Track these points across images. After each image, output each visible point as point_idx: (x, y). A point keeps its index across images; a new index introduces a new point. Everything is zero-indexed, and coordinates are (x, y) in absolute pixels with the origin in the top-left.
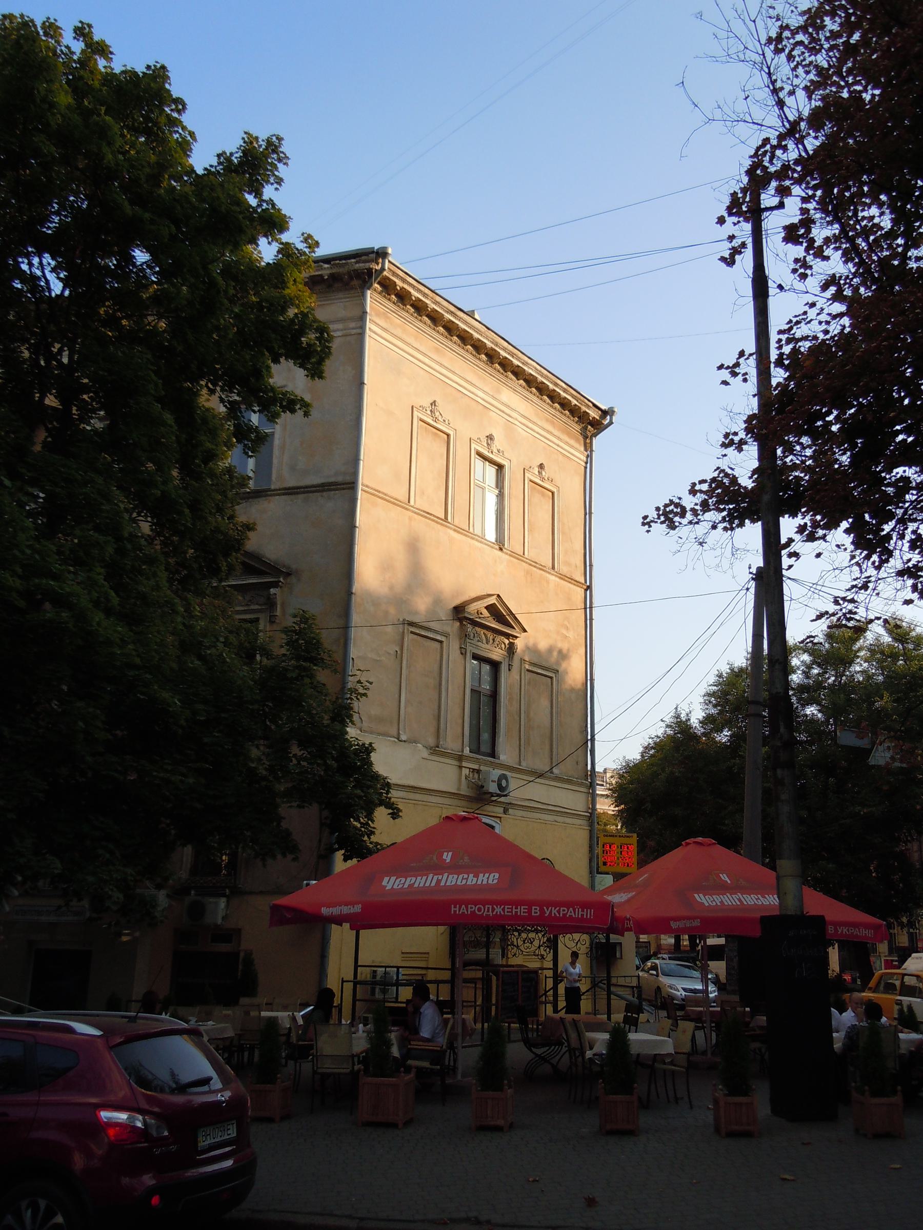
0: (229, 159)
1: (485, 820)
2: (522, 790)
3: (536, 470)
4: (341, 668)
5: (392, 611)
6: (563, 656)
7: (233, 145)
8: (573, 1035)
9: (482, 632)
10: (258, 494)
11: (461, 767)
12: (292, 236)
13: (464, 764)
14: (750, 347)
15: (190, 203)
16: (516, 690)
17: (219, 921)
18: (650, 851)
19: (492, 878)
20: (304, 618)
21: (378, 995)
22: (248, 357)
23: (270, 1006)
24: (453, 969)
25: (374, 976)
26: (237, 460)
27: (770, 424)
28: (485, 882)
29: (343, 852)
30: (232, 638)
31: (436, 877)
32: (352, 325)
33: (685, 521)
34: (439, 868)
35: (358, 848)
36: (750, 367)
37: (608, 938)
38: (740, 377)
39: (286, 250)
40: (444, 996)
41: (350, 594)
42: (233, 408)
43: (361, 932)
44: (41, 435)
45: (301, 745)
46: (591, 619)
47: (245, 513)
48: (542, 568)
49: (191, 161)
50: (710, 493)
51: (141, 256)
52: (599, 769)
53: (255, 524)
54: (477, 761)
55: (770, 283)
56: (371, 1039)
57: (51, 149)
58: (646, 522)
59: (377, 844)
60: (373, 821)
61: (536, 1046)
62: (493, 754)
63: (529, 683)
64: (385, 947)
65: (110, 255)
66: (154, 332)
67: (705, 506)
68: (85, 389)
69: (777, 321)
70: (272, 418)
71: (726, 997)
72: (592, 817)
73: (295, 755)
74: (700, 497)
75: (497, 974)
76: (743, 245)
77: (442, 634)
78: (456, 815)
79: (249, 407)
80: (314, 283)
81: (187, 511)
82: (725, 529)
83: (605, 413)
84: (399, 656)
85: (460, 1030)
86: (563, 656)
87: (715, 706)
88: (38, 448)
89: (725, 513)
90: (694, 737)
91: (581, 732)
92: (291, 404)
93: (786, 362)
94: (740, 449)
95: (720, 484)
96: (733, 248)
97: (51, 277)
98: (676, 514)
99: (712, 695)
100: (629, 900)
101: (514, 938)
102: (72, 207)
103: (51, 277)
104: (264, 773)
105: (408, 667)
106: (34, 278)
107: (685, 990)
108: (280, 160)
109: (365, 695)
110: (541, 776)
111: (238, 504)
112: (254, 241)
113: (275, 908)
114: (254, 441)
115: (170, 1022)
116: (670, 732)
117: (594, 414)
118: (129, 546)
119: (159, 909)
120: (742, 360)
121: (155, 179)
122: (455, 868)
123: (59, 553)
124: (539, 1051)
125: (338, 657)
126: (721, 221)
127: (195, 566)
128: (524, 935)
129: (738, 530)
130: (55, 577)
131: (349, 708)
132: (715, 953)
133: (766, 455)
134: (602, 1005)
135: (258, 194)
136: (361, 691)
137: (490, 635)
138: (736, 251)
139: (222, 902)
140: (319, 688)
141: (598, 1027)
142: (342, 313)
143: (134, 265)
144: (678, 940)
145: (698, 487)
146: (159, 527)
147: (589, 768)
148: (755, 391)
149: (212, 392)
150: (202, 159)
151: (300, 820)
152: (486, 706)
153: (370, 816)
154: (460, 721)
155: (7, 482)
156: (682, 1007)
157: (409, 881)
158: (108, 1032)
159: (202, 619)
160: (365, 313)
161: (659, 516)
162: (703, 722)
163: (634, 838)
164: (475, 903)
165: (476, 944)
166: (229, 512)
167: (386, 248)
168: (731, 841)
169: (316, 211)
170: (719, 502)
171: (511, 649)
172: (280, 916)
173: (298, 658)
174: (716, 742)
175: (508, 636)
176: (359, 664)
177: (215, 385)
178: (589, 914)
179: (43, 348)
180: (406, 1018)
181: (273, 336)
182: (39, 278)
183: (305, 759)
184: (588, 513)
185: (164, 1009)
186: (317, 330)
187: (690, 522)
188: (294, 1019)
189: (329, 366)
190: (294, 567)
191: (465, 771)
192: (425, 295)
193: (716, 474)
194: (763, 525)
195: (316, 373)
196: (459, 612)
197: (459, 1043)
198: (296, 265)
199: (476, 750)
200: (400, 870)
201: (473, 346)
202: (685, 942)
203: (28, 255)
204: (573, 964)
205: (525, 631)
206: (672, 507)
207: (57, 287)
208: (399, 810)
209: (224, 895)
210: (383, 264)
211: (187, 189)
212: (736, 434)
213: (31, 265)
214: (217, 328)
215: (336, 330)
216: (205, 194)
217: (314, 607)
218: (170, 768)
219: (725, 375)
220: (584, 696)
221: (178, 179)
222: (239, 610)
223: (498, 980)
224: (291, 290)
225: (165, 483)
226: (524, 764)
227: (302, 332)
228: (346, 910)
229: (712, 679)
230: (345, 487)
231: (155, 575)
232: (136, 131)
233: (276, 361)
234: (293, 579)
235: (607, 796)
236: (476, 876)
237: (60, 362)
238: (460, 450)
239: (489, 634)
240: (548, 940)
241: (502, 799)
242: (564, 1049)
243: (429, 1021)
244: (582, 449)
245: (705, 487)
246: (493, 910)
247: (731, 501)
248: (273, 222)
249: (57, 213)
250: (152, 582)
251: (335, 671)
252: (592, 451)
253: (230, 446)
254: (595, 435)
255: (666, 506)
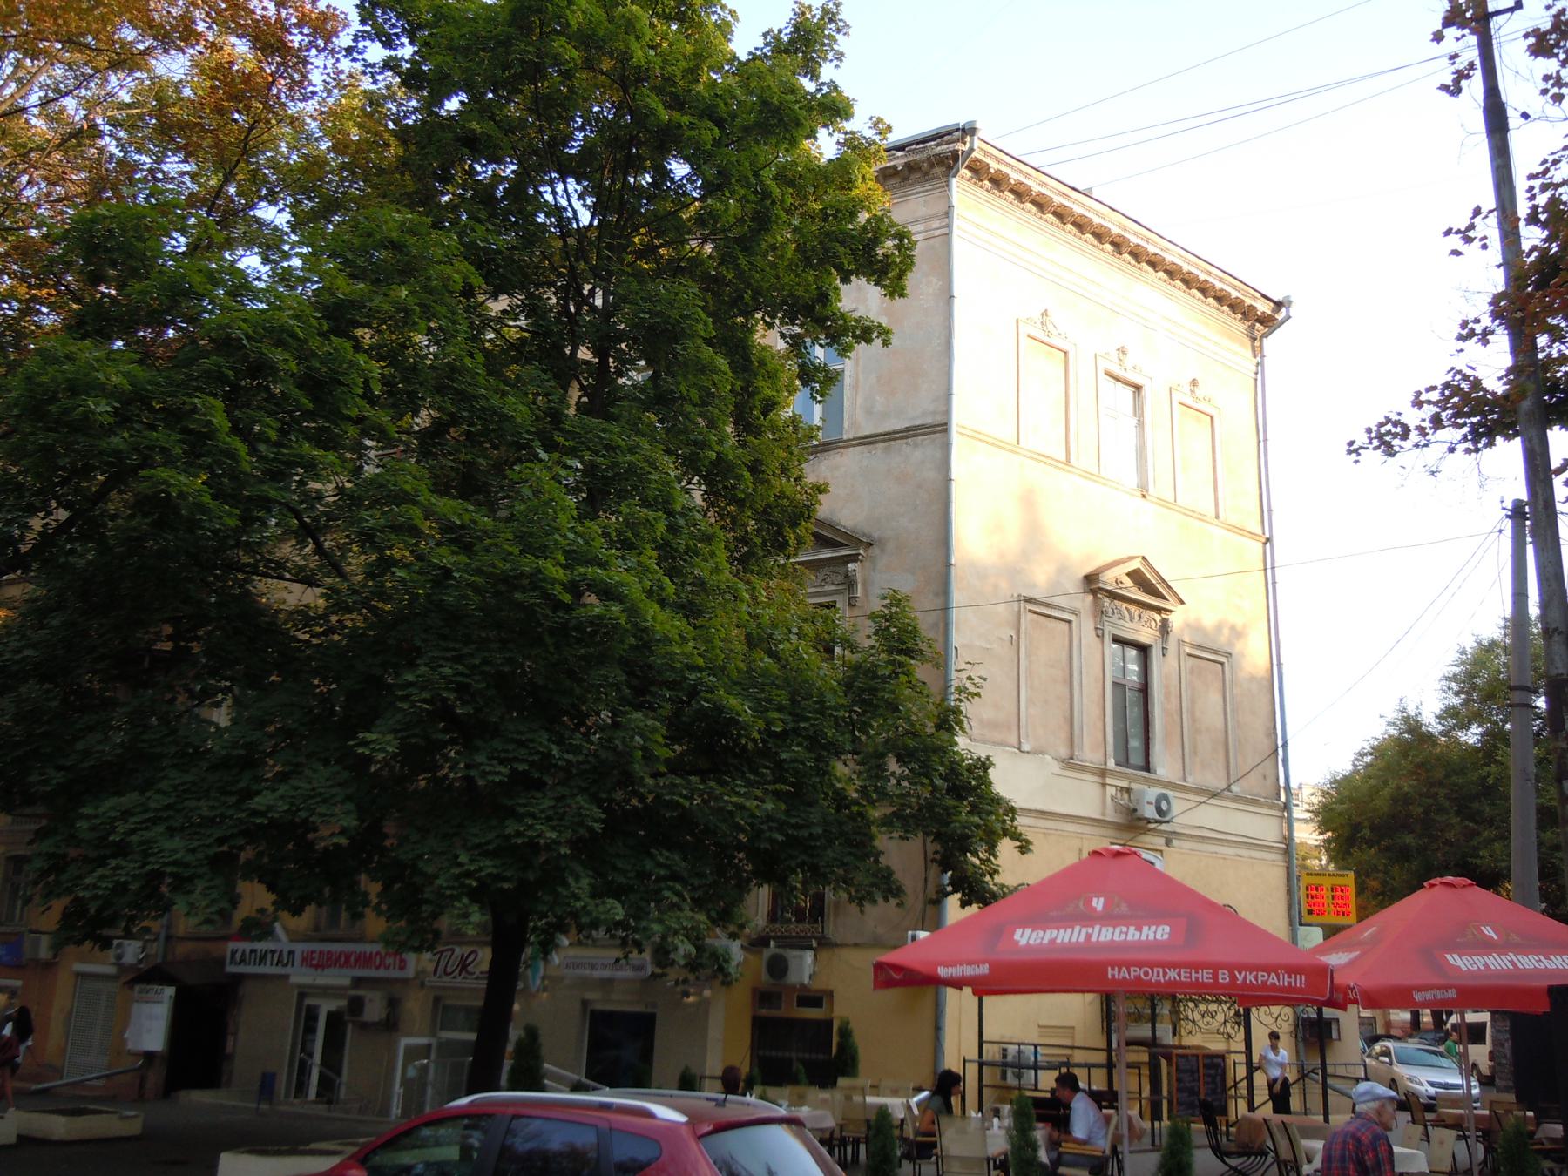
0: (777, 39)
1: (1145, 855)
2: (1186, 814)
3: (1187, 387)
4: (941, 662)
5: (1004, 584)
6: (1237, 633)
7: (780, 19)
8: (1283, 1144)
9: (1123, 606)
10: (827, 447)
11: (1104, 785)
12: (859, 123)
13: (1109, 781)
14: (1489, 201)
15: (734, 97)
16: (1175, 682)
17: (806, 981)
18: (1379, 893)
19: (1162, 932)
20: (896, 600)
21: (1011, 1080)
22: (811, 279)
23: (876, 1089)
24: (1109, 1049)
25: (1005, 1056)
26: (800, 406)
27: (1528, 301)
28: (1151, 937)
29: (959, 895)
30: (809, 629)
31: (1084, 931)
32: (936, 224)
33: (1408, 444)
34: (1089, 918)
35: (975, 891)
36: (1489, 228)
37: (1320, 1012)
38: (1477, 243)
39: (852, 143)
40: (1099, 1084)
41: (948, 565)
42: (796, 344)
43: (986, 999)
44: (575, 393)
45: (900, 759)
46: (1274, 583)
47: (816, 471)
48: (1202, 518)
49: (732, 46)
50: (1443, 403)
51: (679, 169)
52: (1294, 785)
53: (827, 484)
54: (1126, 777)
55: (1510, 113)
56: (1011, 1137)
57: (572, 54)
58: (1353, 450)
59: (1003, 886)
60: (996, 857)
61: (1229, 1154)
62: (1147, 767)
63: (1192, 672)
64: (1019, 1020)
65: (639, 171)
66: (697, 262)
67: (1437, 422)
68: (621, 337)
69: (1524, 162)
70: (844, 352)
71: (1493, 1095)
72: (1288, 847)
73: (893, 773)
74: (1429, 410)
75: (1168, 1057)
76: (1472, 66)
77: (1070, 612)
78: (1107, 850)
79: (815, 340)
80: (886, 176)
81: (747, 474)
82: (1468, 451)
83: (1278, 305)
84: (1015, 642)
85: (1125, 1131)
86: (1237, 633)
87: (1457, 694)
88: (572, 411)
89: (1466, 430)
90: (1430, 737)
91: (1268, 736)
92: (866, 332)
93: (1543, 217)
94: (1484, 341)
95: (1457, 391)
96: (1458, 72)
97: (577, 205)
98: (1395, 435)
99: (1454, 678)
100: (1351, 963)
101: (1189, 1010)
102: (597, 119)
103: (577, 205)
104: (855, 795)
105: (1028, 656)
106: (558, 210)
107: (1432, 1084)
108: (839, 31)
109: (978, 695)
110: (1215, 795)
111: (806, 461)
112: (812, 135)
113: (879, 967)
114: (820, 381)
115: (755, 1106)
116: (1393, 731)
117: (1263, 307)
118: (682, 522)
119: (734, 964)
120: (1477, 221)
121: (693, 73)
122: (1109, 918)
123: (605, 535)
124: (1234, 1162)
125: (938, 646)
126: (1438, 37)
127: (758, 541)
128: (1202, 1007)
129: (1486, 452)
130: (603, 565)
131: (957, 712)
132: (1475, 1034)
133: (1522, 345)
134: (1315, 1100)
135: (814, 75)
136: (972, 689)
137: (1134, 610)
138: (1461, 75)
139: (809, 957)
140: (918, 688)
141: (1311, 1133)
142: (923, 211)
143: (672, 179)
144: (1416, 1016)
145: (1424, 397)
146: (711, 495)
147: (1282, 783)
148: (1499, 260)
149: (770, 326)
150: (745, 42)
151: (902, 854)
152: (1136, 706)
153: (992, 849)
154: (1100, 725)
155: (543, 455)
156: (1430, 1108)
157: (1050, 935)
158: (694, 1119)
159: (769, 606)
160: (951, 207)
161: (1371, 439)
162: (1441, 717)
163: (1349, 879)
164: (1140, 965)
165: (1138, 1018)
166: (795, 473)
167: (973, 122)
168: (1490, 880)
169: (884, 86)
170: (1456, 415)
171: (1164, 628)
172: (890, 977)
173: (890, 651)
174: (1460, 744)
175: (1159, 610)
176: (965, 655)
177: (773, 317)
178: (1299, 981)
179: (571, 291)
180: (1054, 1111)
181: (842, 250)
182: (565, 209)
183: (906, 778)
184: (1262, 441)
185: (749, 1087)
186: (895, 236)
187: (1417, 446)
188: (909, 1108)
189: (912, 280)
190: (876, 535)
191: (1111, 791)
192: (1027, 176)
193: (1449, 378)
194: (1523, 442)
195: (896, 290)
196: (1091, 582)
197: (1124, 1148)
198: (864, 158)
199: (1124, 761)
200: (1037, 921)
201: (1094, 234)
202: (1426, 1017)
203: (551, 183)
204: (1274, 1048)
205: (1182, 602)
206: (1389, 427)
207: (585, 218)
208: (1028, 842)
209: (810, 948)
210: (972, 142)
211: (731, 81)
212: (1477, 321)
213: (554, 193)
214: (774, 248)
215: (917, 231)
216: (752, 85)
217: (905, 584)
218: (743, 791)
219: (1455, 241)
220: (1271, 685)
221: (718, 69)
222: (813, 591)
223: (1169, 1065)
224: (859, 190)
225: (721, 442)
226: (1190, 779)
227: (876, 241)
228: (969, 971)
229: (1454, 656)
230: (935, 430)
231: (713, 554)
232: (667, 18)
233: (846, 280)
234: (875, 551)
235: (1306, 821)
236: (1139, 929)
237: (593, 308)
238: (1083, 371)
239: (1133, 609)
240: (1237, 1014)
241: (1163, 827)
242: (1270, 1160)
243: (1083, 1117)
244: (1249, 352)
245: (1435, 396)
246: (1165, 974)
247: (1479, 414)
248: (834, 108)
249: (582, 128)
250: (711, 564)
251: (938, 666)
252: (1263, 357)
253: (792, 390)
254: (1266, 335)
255: (1381, 425)
